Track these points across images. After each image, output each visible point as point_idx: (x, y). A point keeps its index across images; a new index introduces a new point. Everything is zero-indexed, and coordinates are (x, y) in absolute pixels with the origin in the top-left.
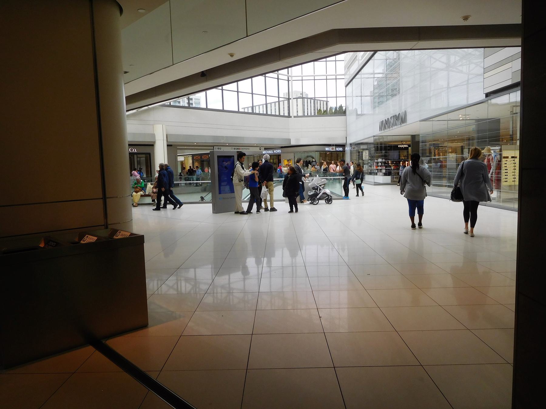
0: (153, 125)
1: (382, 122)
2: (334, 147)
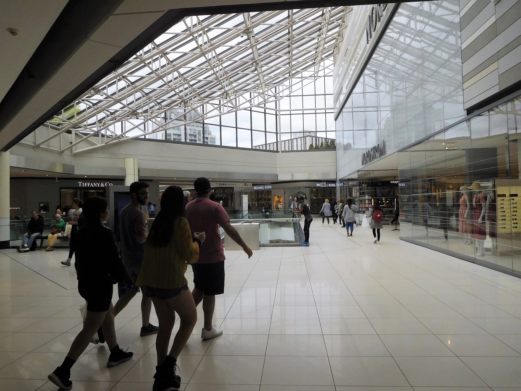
1: (364, 155)
2: (325, 183)
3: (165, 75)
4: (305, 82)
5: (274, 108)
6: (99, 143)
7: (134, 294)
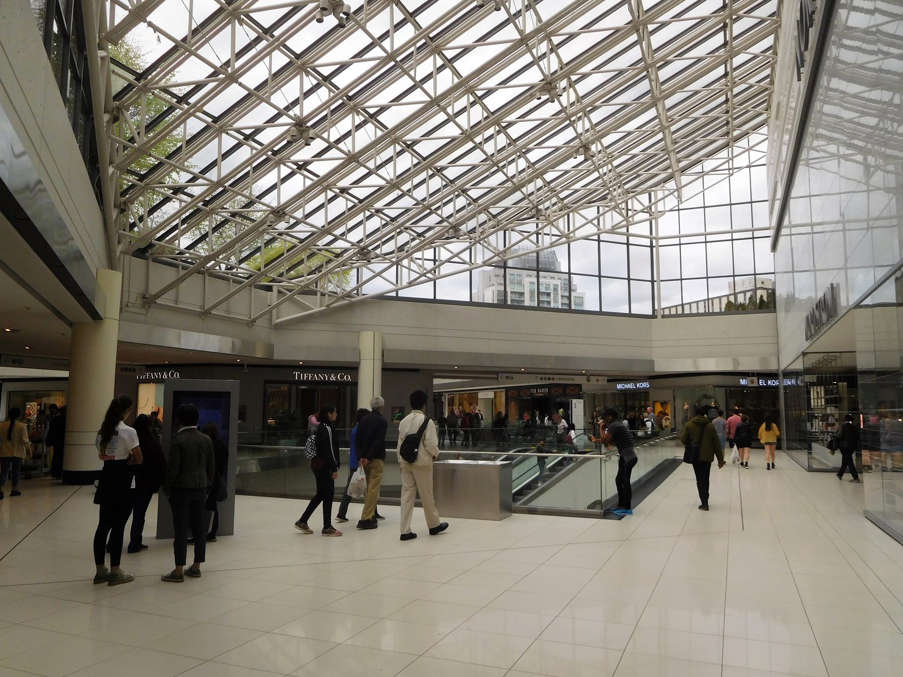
0: (359, 332)
2: (755, 379)
3: (523, 186)
4: (709, 180)
5: (648, 234)
6: (315, 305)
7: (639, 481)
